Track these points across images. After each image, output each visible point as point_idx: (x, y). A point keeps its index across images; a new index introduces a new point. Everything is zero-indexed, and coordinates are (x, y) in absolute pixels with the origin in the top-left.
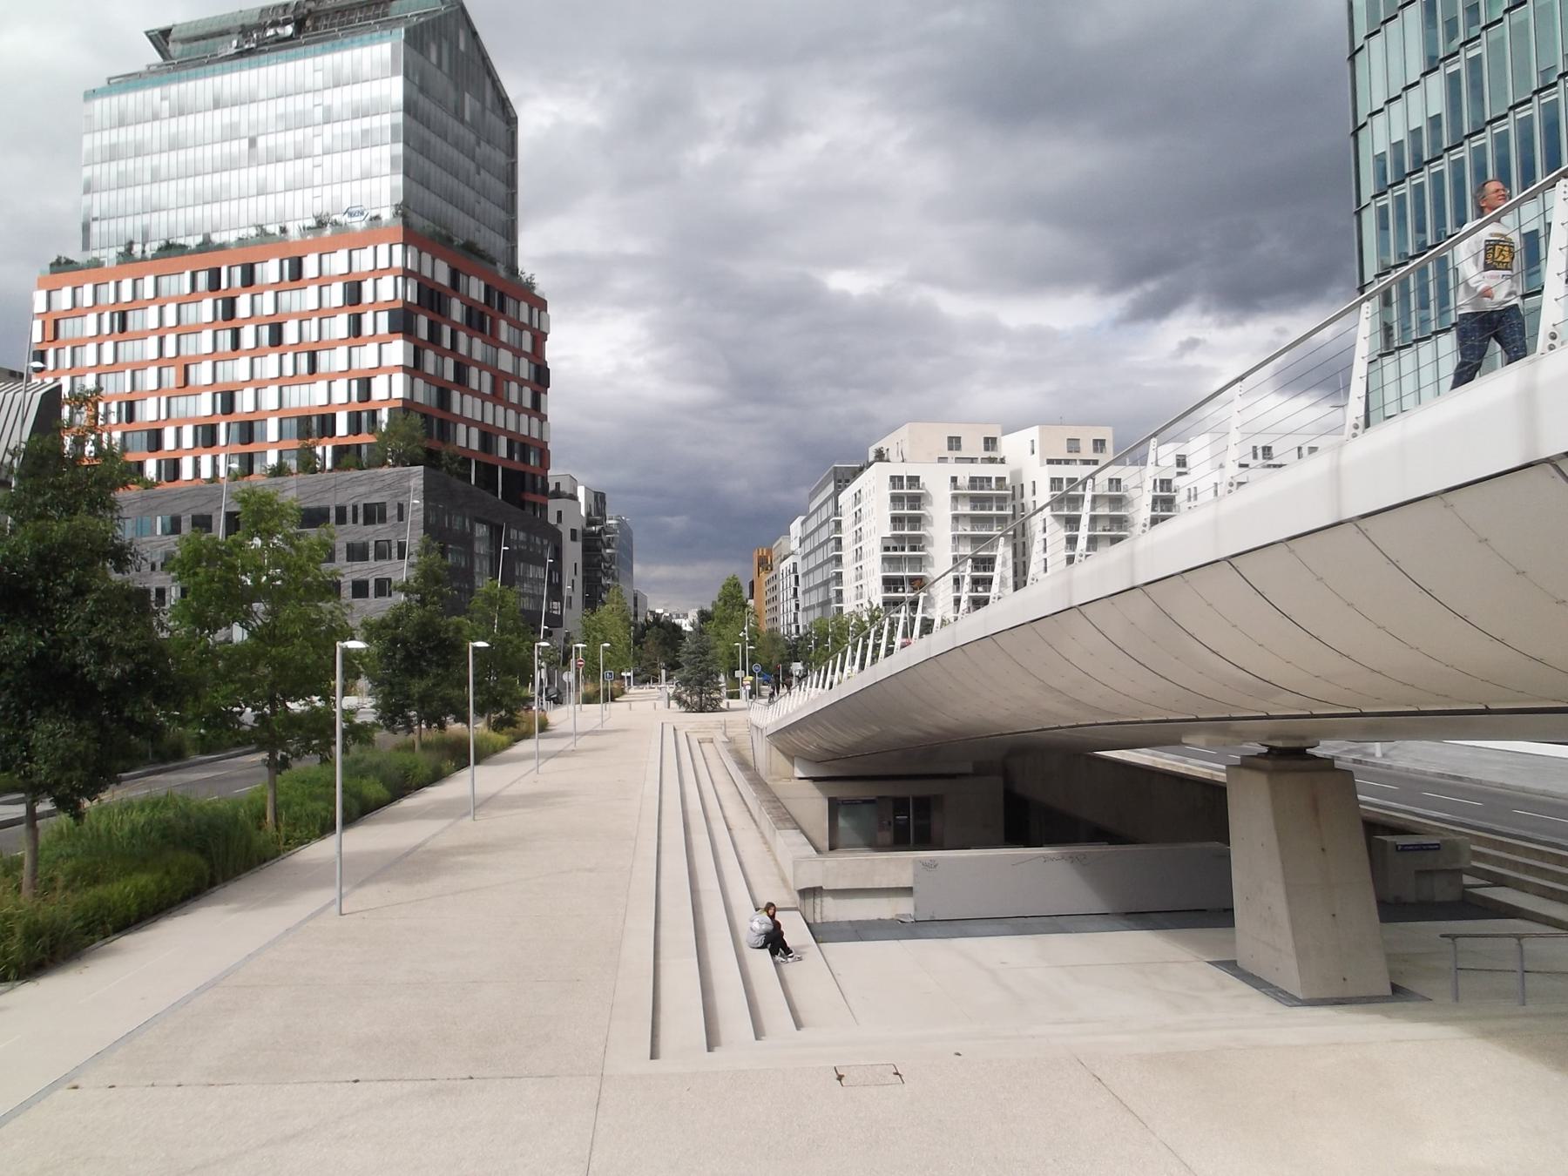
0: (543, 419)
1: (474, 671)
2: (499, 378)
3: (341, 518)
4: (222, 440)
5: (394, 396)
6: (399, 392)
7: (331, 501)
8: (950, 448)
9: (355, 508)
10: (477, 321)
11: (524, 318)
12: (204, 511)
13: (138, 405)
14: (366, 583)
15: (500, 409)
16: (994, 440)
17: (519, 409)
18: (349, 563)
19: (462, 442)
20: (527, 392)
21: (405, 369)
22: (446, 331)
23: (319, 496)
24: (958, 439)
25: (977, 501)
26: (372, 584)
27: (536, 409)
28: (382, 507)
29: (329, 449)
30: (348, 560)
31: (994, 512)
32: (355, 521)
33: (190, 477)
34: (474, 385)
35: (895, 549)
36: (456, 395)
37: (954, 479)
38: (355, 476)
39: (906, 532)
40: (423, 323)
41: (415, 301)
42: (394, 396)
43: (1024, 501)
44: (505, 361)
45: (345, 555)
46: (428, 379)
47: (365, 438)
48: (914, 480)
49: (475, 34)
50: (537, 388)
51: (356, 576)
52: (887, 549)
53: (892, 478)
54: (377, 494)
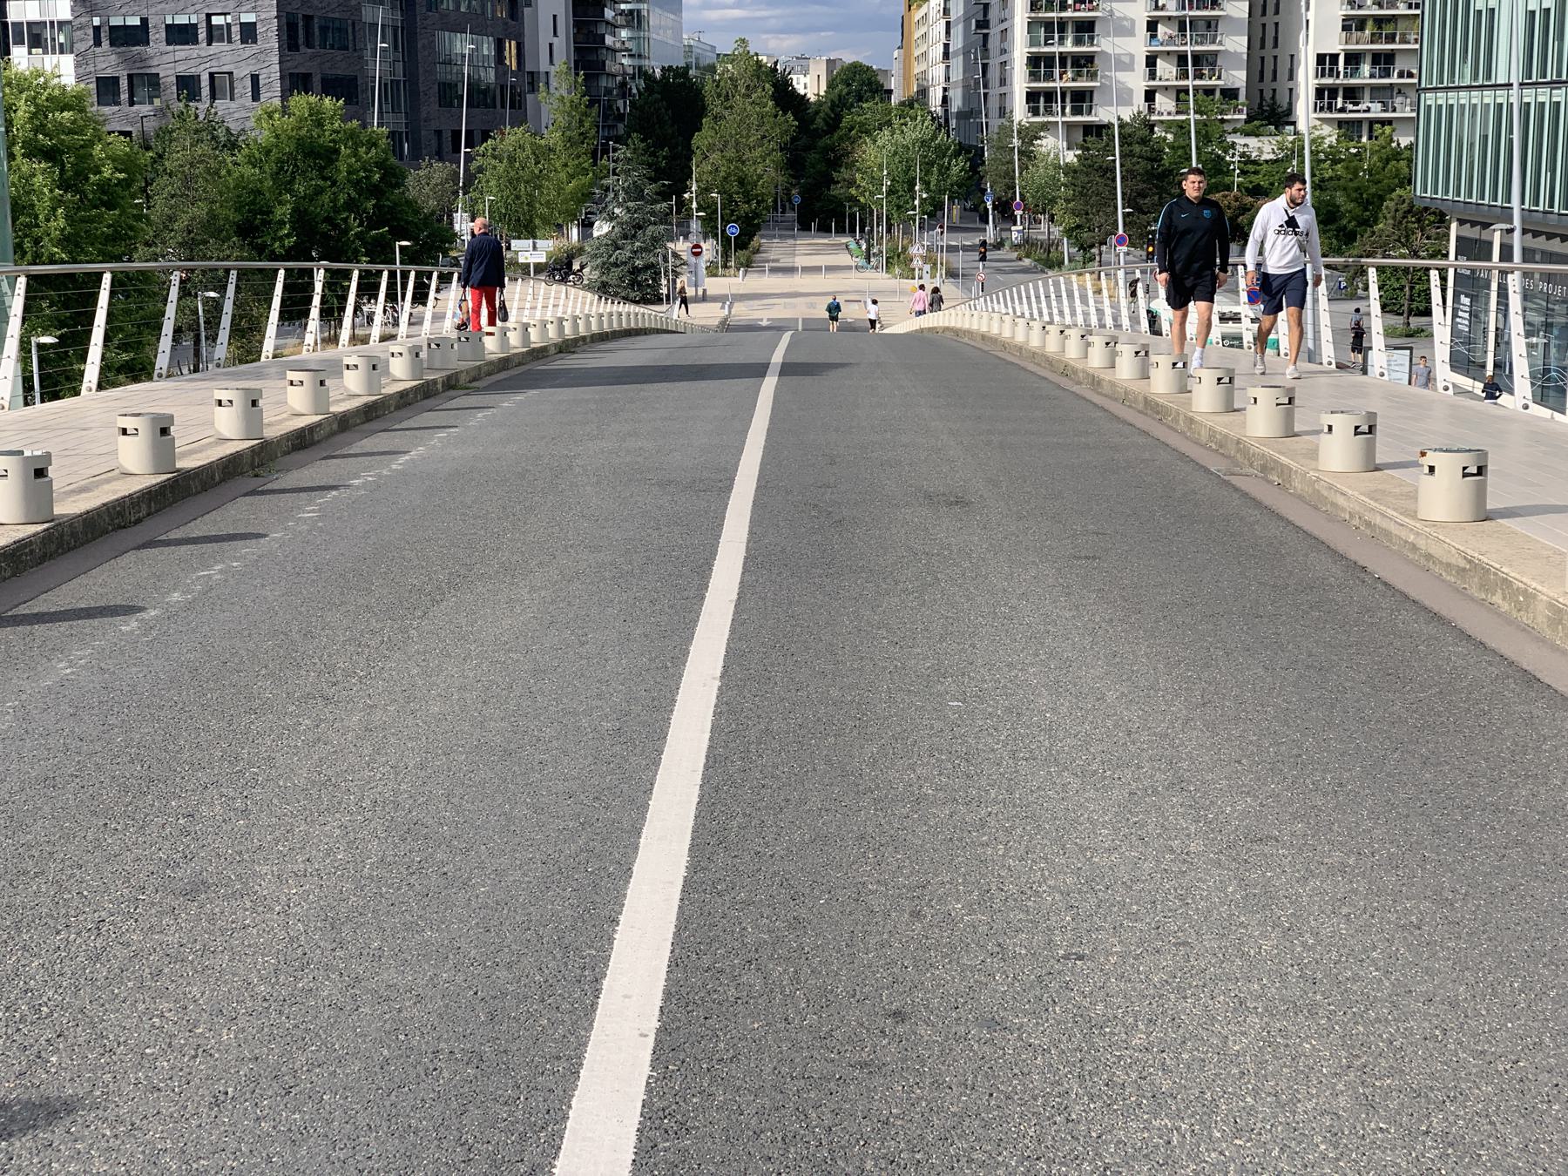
30: (169, 43)
51: (182, 69)
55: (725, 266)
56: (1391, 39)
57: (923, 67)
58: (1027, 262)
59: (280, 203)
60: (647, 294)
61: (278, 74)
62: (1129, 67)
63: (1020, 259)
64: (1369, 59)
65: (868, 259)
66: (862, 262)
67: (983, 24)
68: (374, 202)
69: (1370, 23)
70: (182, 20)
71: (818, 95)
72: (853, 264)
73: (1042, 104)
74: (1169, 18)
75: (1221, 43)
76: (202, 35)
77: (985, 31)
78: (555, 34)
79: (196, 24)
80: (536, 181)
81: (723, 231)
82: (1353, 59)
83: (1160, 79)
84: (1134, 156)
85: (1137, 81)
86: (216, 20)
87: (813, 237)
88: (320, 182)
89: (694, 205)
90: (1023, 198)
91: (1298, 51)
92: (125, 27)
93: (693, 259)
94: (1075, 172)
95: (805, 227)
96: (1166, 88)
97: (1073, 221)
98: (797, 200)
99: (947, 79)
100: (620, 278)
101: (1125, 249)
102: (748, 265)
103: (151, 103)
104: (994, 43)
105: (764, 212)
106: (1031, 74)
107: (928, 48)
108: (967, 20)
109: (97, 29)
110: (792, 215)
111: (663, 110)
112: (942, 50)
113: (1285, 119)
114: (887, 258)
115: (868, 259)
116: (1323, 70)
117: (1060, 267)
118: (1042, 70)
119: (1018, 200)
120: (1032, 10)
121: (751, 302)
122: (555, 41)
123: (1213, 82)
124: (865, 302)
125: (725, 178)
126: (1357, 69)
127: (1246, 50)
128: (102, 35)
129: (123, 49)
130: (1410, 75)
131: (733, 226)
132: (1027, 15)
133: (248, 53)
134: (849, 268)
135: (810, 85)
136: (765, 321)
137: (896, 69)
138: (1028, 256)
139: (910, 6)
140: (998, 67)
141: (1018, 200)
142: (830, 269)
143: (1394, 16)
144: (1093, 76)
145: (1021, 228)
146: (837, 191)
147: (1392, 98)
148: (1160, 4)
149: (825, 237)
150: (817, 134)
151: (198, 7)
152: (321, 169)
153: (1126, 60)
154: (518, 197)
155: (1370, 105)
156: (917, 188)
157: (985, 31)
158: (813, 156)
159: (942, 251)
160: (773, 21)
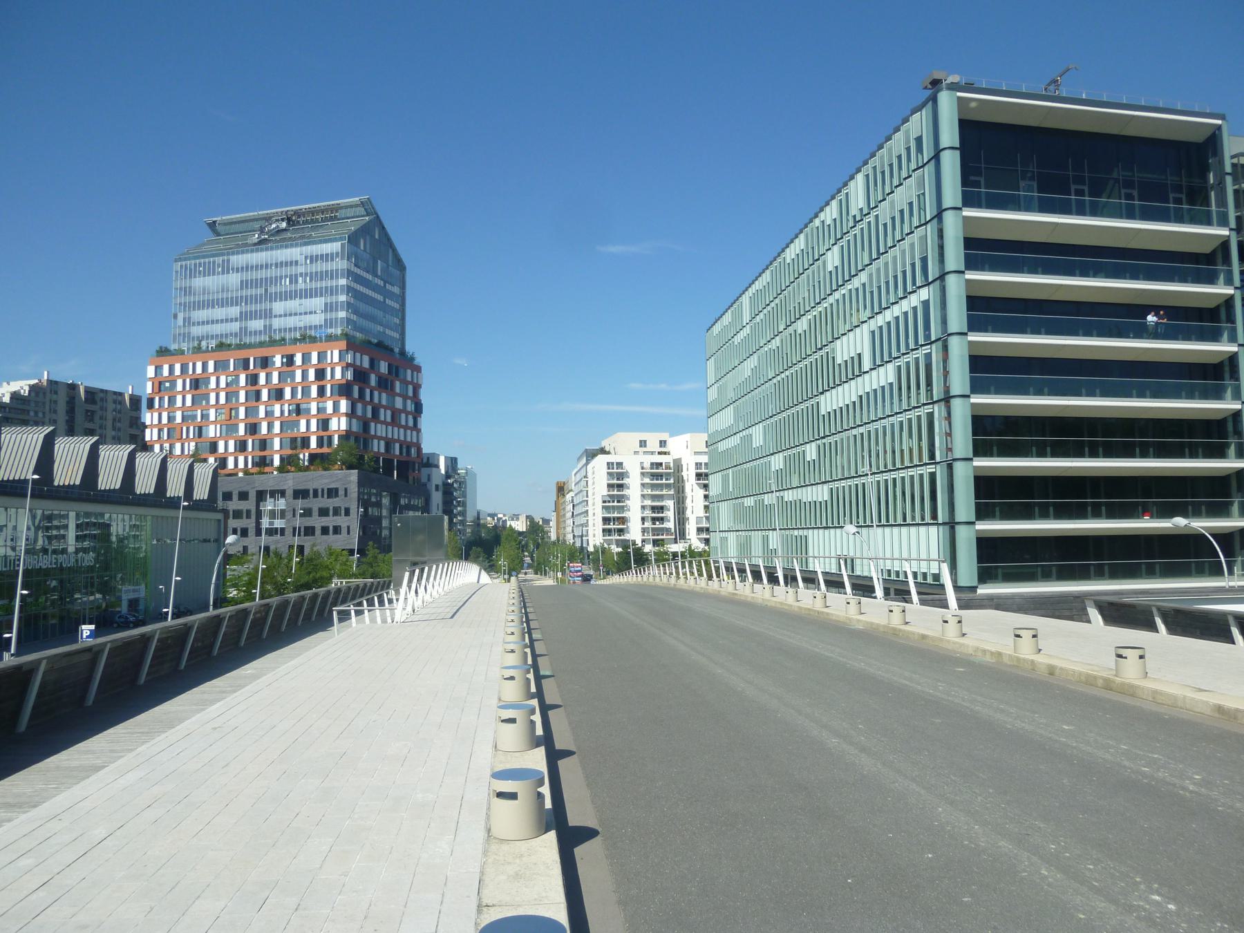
0: (419, 431)
1: (13, 618)
2: (395, 414)
3: (316, 495)
4: (250, 449)
5: (341, 429)
6: (343, 427)
8: (641, 446)
9: (323, 490)
10: (385, 384)
11: (409, 379)
12: (245, 489)
13: (204, 428)
14: (328, 527)
15: (396, 429)
17: (406, 427)
19: (376, 449)
20: (410, 417)
21: (347, 415)
22: (368, 391)
24: (645, 441)
25: (654, 476)
26: (331, 528)
27: (416, 427)
28: (337, 490)
29: (307, 454)
31: (664, 481)
32: (323, 496)
33: (157, 423)
34: (382, 418)
35: (609, 502)
36: (373, 425)
39: (615, 493)
40: (356, 388)
41: (352, 379)
42: (341, 429)
43: (683, 474)
44: (399, 403)
46: (358, 418)
47: (325, 450)
48: (620, 465)
49: (383, 228)
51: (323, 524)
52: (604, 502)
53: (608, 463)
54: (333, 484)
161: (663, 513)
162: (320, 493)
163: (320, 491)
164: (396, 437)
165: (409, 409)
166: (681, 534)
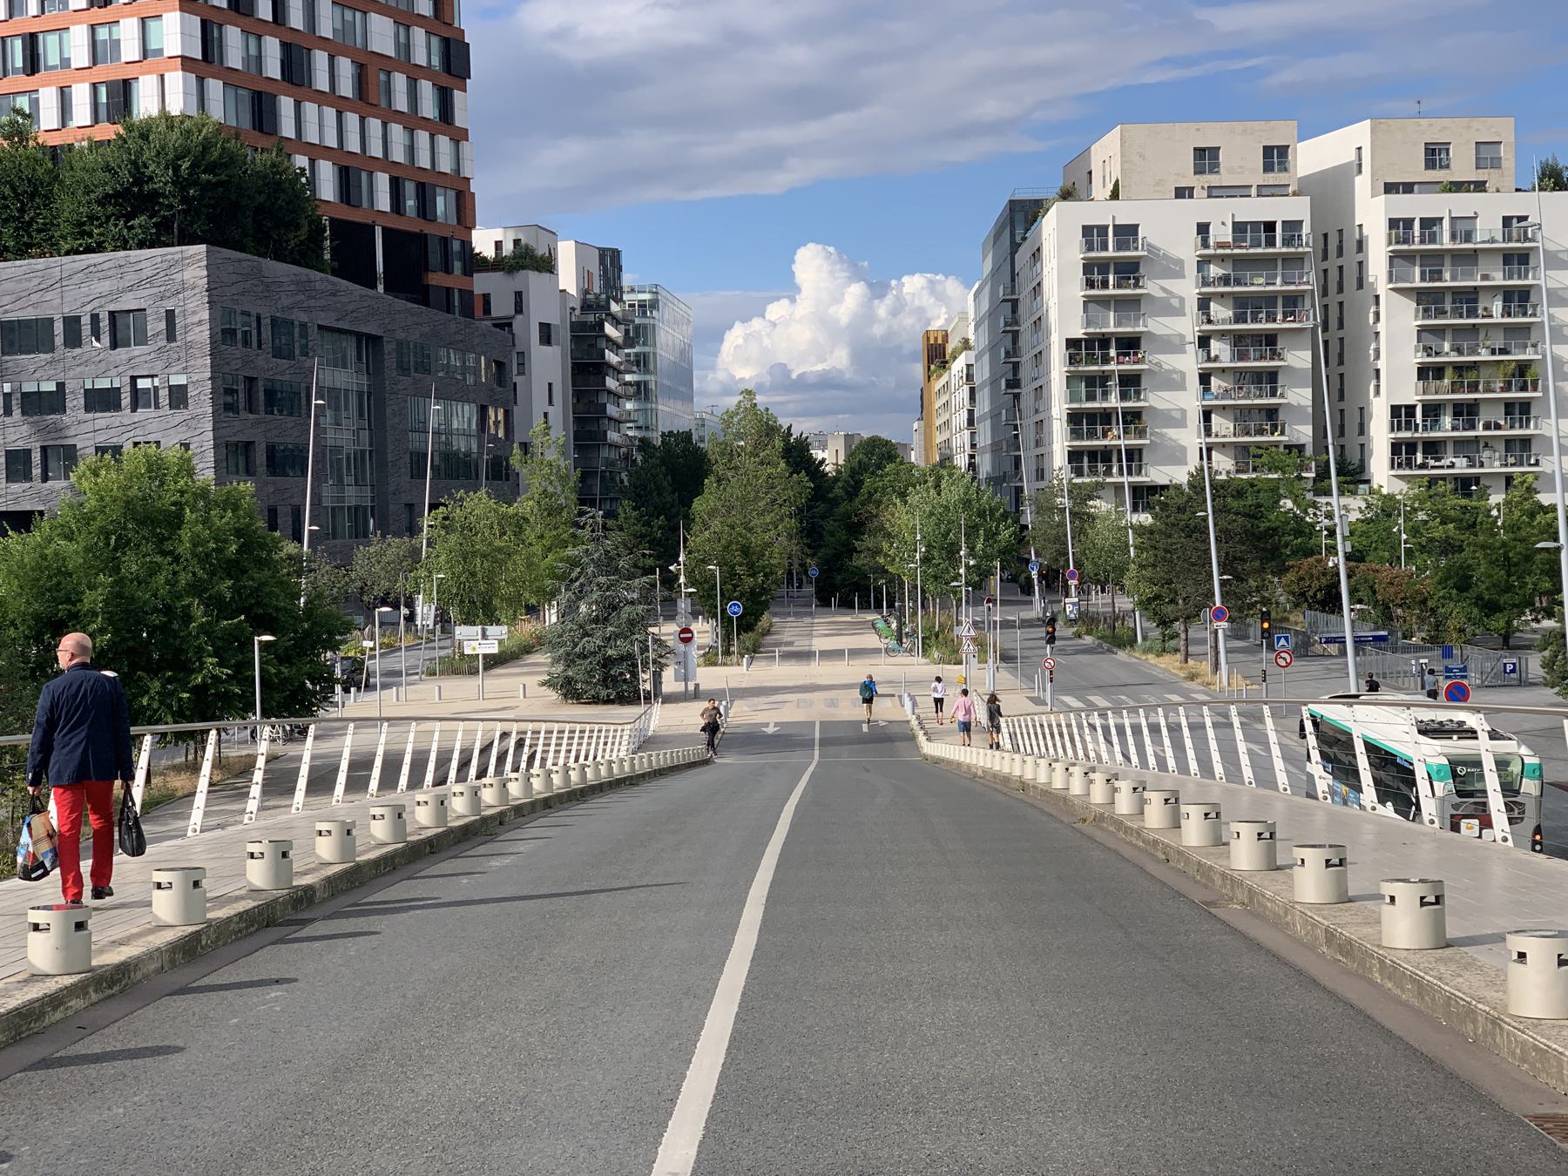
0: (459, 136)
2: (369, 69)
7: (55, 307)
8: (1199, 171)
9: (95, 318)
15: (374, 125)
16: (1283, 151)
17: (412, 122)
18: (90, 416)
20: (426, 89)
21: (186, 63)
23: (34, 298)
24: (1215, 151)
34: (321, 82)
36: (286, 105)
37: (1203, 229)
38: (92, 262)
45: (82, 401)
46: (231, 78)
48: (1127, 233)
50: (446, 81)
51: (101, 439)
53: (1087, 231)
54: (131, 295)
55: (727, 653)
56: (1474, 387)
57: (945, 436)
58: (1088, 640)
59: (92, 587)
60: (623, 691)
61: (212, 442)
62: (1181, 423)
63: (1080, 637)
64: (1450, 410)
65: (900, 641)
66: (893, 643)
67: (1014, 383)
68: (230, 583)
69: (1449, 372)
70: (103, 384)
71: (837, 464)
72: (883, 646)
73: (1086, 464)
74: (1223, 370)
75: (1282, 396)
76: (126, 400)
77: (1016, 391)
78: (550, 403)
79: (119, 388)
80: (497, 558)
81: (723, 611)
82: (1433, 411)
83: (1217, 436)
84: (1229, 512)
85: (1190, 438)
86: (142, 384)
87: (833, 615)
88: (159, 559)
89: (682, 580)
90: (1078, 565)
91: (1369, 403)
92: (39, 393)
93: (682, 647)
94: (1152, 532)
95: (824, 602)
96: (1224, 445)
97: (1149, 591)
98: (814, 572)
99: (973, 446)
100: (588, 673)
101: (1224, 624)
102: (754, 650)
103: (67, 477)
104: (1027, 400)
105: (773, 587)
106: (1073, 432)
107: (951, 416)
108: (994, 382)
109: (7, 396)
110: (810, 590)
111: (661, 476)
112: (966, 416)
113: (1357, 477)
114: (923, 638)
115: (900, 641)
116: (1399, 423)
117: (1132, 646)
118: (1085, 427)
119: (1071, 568)
120: (1070, 363)
121: (756, 700)
122: (550, 410)
123: (1276, 438)
124: (900, 697)
125: (726, 548)
126: (1437, 421)
127: (1310, 403)
128: (14, 402)
129: (36, 418)
130: (1498, 427)
131: (735, 604)
132: (1066, 369)
133: (179, 419)
134: (877, 651)
135: (830, 457)
136: (772, 725)
137: (917, 441)
138: (1089, 633)
139: (929, 377)
140: (1033, 427)
141: (1071, 568)
142: (856, 653)
143: (1475, 362)
144: (1141, 433)
145: (1077, 600)
146: (859, 561)
147: (1478, 452)
148: (1212, 355)
149: (847, 615)
150: (835, 502)
151: (121, 369)
152: (162, 540)
153: (1178, 415)
154: (473, 574)
155: (1454, 460)
156: (962, 553)
157: (1016, 391)
158: (829, 525)
159: (995, 628)
160: (791, 406)
161: (1273, 394)
162: (86, 329)
163: (86, 320)
164: (376, 150)
165: (420, 57)
166: (1354, 475)
